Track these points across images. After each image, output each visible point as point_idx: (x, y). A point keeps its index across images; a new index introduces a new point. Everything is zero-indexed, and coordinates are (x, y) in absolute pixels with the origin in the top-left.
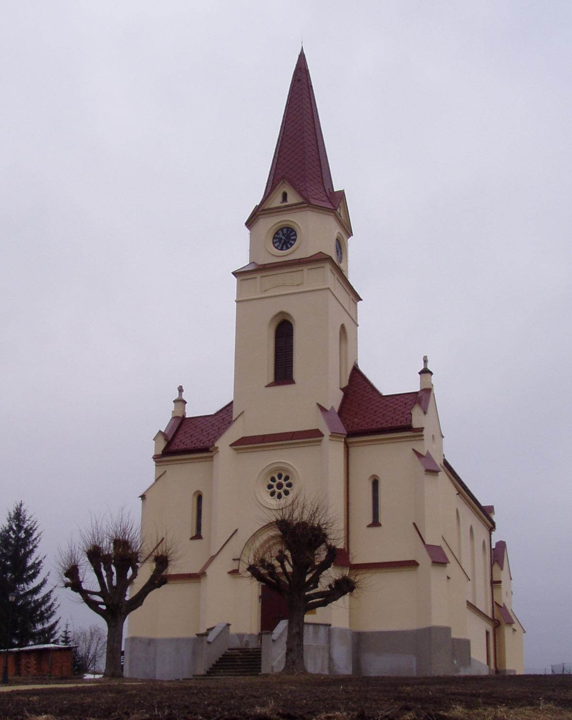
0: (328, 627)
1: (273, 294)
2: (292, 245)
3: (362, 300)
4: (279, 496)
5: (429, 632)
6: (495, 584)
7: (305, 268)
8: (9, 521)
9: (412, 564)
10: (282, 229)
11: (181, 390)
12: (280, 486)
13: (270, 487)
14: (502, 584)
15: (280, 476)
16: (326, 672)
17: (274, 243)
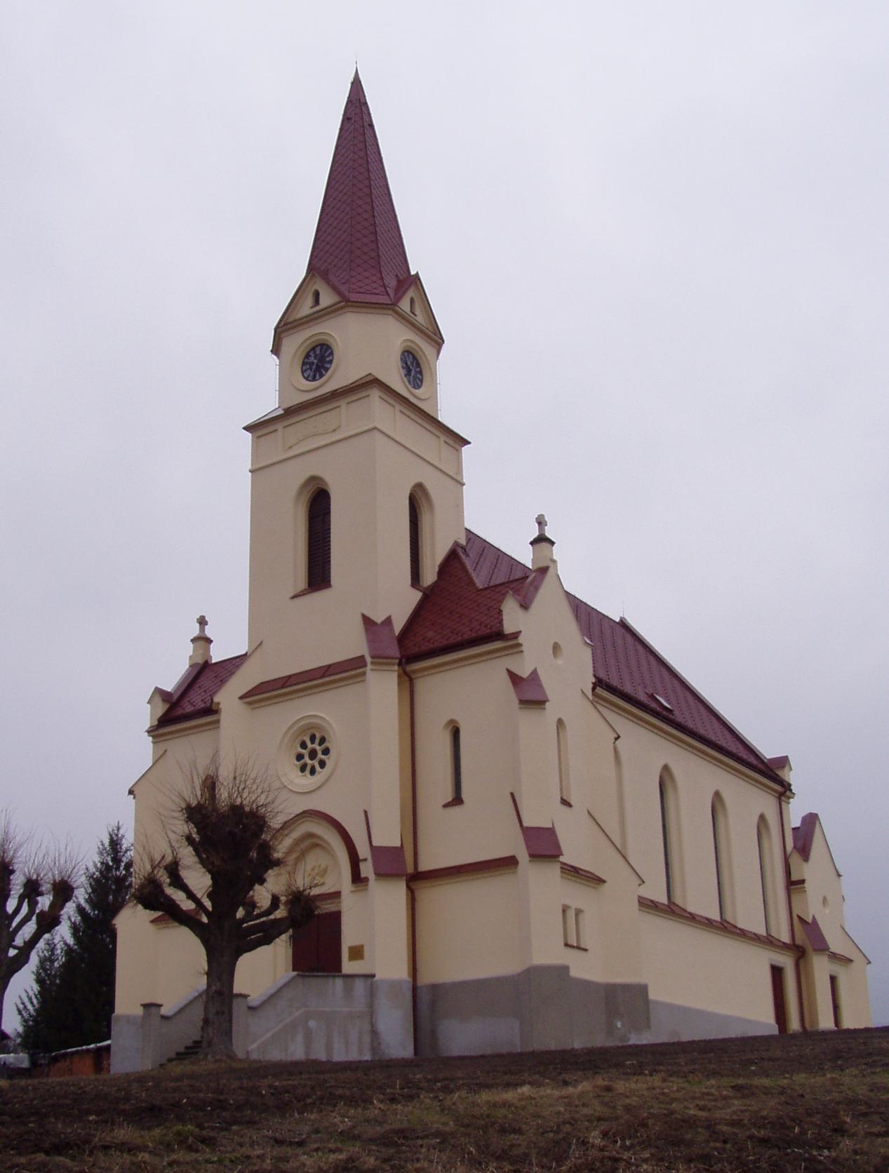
0: (369, 981)
1: (301, 451)
2: (327, 370)
3: (466, 442)
4: (313, 772)
5: (533, 974)
6: (794, 885)
7: (343, 403)
8: (101, 854)
9: (509, 863)
10: (313, 349)
11: (202, 622)
12: (313, 755)
13: (300, 757)
14: (806, 885)
15: (313, 738)
16: (367, 1057)
17: (303, 372)
